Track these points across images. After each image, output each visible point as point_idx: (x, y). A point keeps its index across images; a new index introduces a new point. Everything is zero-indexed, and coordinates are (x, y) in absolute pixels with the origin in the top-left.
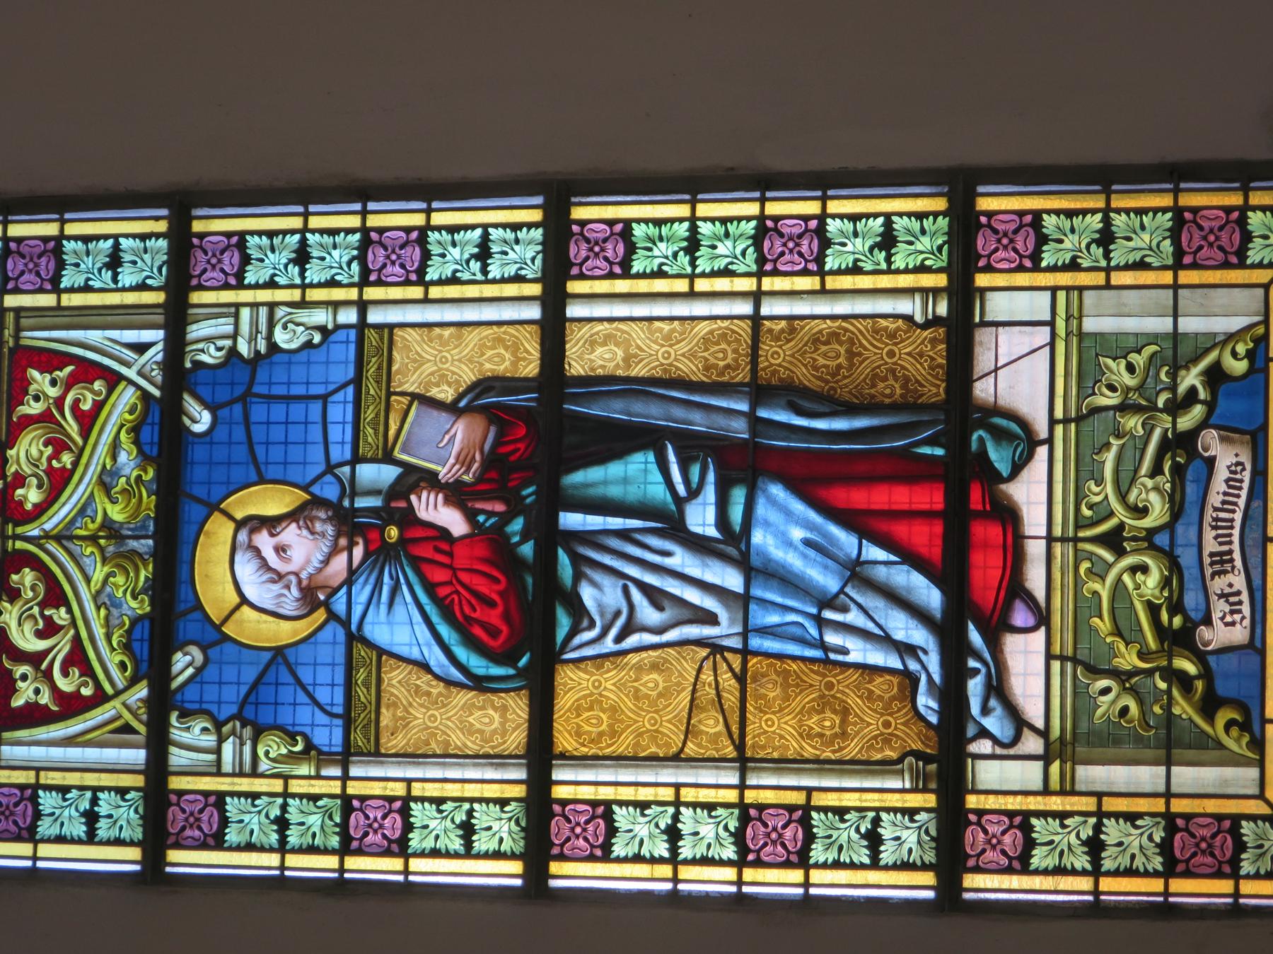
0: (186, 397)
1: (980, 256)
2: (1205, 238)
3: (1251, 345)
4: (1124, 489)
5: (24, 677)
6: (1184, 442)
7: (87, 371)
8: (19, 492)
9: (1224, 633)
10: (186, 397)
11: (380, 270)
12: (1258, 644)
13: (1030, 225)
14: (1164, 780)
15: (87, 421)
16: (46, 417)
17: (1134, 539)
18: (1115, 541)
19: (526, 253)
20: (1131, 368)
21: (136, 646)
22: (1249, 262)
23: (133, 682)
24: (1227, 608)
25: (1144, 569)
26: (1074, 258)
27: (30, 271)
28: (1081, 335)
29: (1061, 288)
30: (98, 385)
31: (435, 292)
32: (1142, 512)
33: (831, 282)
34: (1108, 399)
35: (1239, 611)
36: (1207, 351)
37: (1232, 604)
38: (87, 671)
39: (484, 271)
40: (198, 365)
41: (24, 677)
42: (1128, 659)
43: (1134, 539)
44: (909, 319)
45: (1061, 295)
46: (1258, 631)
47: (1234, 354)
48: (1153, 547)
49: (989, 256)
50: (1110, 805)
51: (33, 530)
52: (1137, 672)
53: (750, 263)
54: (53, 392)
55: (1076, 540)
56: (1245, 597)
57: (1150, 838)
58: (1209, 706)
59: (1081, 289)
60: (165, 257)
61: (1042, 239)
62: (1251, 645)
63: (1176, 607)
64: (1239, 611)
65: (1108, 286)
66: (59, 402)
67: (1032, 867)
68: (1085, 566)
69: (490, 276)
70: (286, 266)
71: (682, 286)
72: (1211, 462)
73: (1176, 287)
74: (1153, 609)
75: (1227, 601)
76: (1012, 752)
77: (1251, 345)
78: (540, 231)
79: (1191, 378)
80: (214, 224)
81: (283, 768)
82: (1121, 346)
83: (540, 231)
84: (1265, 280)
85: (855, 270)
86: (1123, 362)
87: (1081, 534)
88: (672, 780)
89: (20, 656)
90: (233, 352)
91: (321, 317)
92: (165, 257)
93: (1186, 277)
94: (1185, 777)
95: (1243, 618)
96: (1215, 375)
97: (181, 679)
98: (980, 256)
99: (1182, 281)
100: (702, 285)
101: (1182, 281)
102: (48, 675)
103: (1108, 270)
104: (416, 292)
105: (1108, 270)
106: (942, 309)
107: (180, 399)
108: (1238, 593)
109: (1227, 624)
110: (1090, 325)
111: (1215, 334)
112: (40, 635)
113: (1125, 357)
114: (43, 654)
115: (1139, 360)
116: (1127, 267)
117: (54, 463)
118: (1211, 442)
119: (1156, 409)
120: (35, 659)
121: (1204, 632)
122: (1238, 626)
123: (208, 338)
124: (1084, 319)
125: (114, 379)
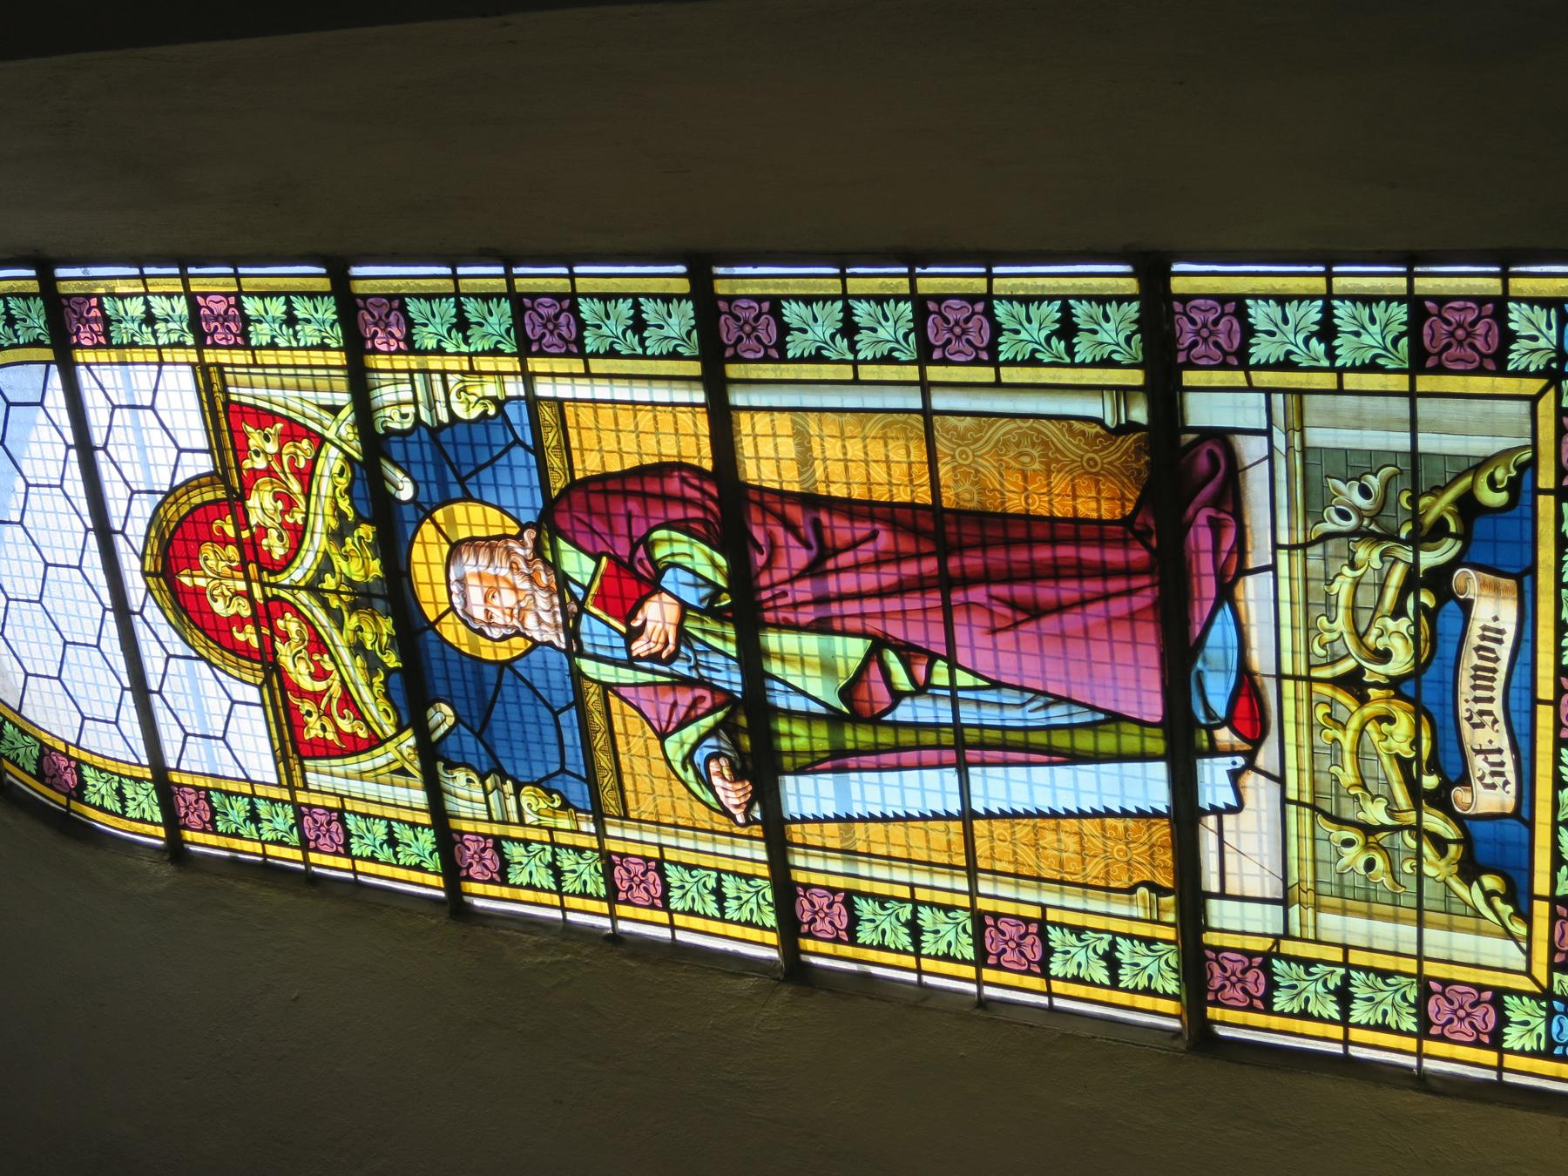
0: (383, 462)
1: (725, 347)
2: (958, 338)
3: (1514, 473)
4: (1362, 629)
5: (309, 714)
6: (1439, 579)
7: (294, 431)
8: (265, 542)
9: (1489, 796)
10: (383, 462)
11: (735, 345)
12: (1525, 814)
13: (1234, 314)
14: (1268, 907)
15: (306, 476)
16: (269, 472)
17: (1377, 685)
18: (1353, 683)
19: (1114, 330)
20: (1365, 492)
21: (393, 694)
22: (1510, 367)
23: (400, 729)
24: (1488, 769)
25: (1391, 720)
26: (819, 349)
27: (754, 329)
28: (1304, 450)
29: (1277, 390)
30: (305, 444)
31: (1008, 374)
32: (1384, 656)
33: (1008, 374)
34: (1333, 524)
35: (1502, 774)
36: (1459, 477)
37: (1493, 764)
38: (360, 716)
39: (1070, 350)
40: (390, 432)
41: (309, 714)
42: (1376, 813)
43: (1377, 685)
44: (1100, 422)
45: (1278, 399)
46: (1525, 802)
47: (1492, 484)
48: (1400, 696)
49: (1440, 354)
50: (1356, 958)
51: (283, 579)
52: (1383, 828)
53: (908, 352)
54: (272, 447)
55: (1310, 680)
56: (1508, 757)
57: (1404, 998)
58: (1469, 871)
59: (1300, 393)
60: (693, 322)
61: (784, 329)
62: (1516, 814)
63: (1434, 766)
64: (1502, 774)
65: (1340, 391)
66: (278, 456)
67: (1276, 1008)
68: (1321, 711)
69: (1078, 359)
70: (624, 333)
71: (846, 372)
72: (1466, 606)
73: (1412, 395)
74: (1403, 764)
75: (1486, 760)
76: (158, 632)
77: (1514, 473)
78: (1135, 305)
79: (1439, 507)
80: (741, 281)
81: (549, 822)
82: (1354, 465)
83: (1135, 305)
84: (1534, 392)
85: (1033, 361)
86: (1356, 484)
87: (1315, 673)
88: (906, 879)
89: (302, 693)
90: (418, 420)
91: (491, 389)
92: (693, 322)
93: (1425, 383)
94: (1436, 940)
95: (1506, 783)
96: (1468, 506)
97: (442, 730)
98: (725, 347)
99: (1420, 388)
100: (867, 372)
101: (1420, 388)
102: (328, 713)
103: (855, 363)
104: (985, 374)
105: (855, 363)
106: (1139, 414)
107: (379, 465)
108: (1500, 751)
109: (1487, 786)
110: (1318, 437)
111: (1468, 457)
112: (314, 677)
113: (1359, 480)
114: (321, 694)
115: (1374, 482)
116: (875, 361)
117: (287, 518)
118: (1468, 582)
119: (1398, 540)
120: (316, 697)
121: (1460, 795)
122: (1499, 790)
123: (395, 402)
124: (1307, 430)
125: (320, 441)
